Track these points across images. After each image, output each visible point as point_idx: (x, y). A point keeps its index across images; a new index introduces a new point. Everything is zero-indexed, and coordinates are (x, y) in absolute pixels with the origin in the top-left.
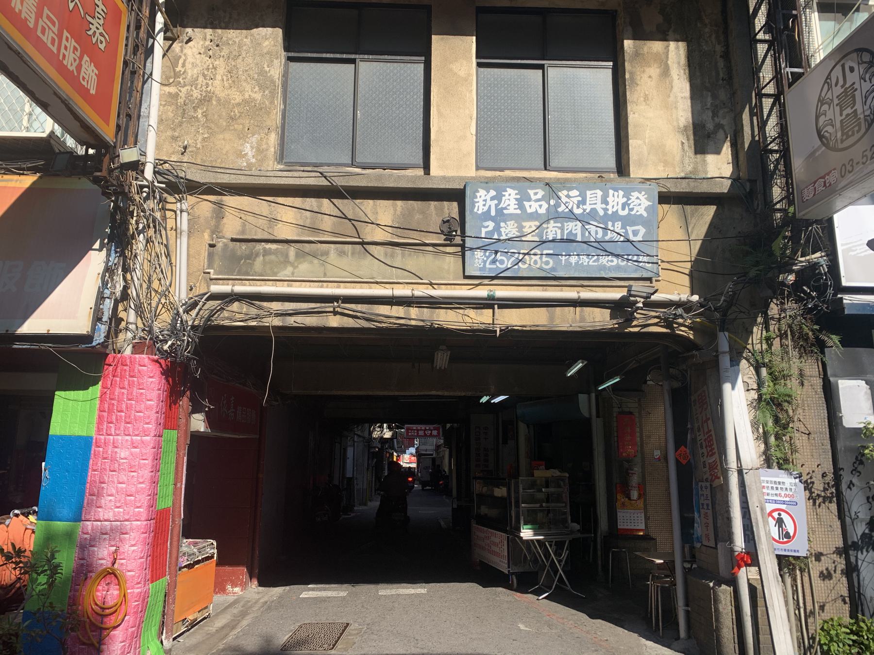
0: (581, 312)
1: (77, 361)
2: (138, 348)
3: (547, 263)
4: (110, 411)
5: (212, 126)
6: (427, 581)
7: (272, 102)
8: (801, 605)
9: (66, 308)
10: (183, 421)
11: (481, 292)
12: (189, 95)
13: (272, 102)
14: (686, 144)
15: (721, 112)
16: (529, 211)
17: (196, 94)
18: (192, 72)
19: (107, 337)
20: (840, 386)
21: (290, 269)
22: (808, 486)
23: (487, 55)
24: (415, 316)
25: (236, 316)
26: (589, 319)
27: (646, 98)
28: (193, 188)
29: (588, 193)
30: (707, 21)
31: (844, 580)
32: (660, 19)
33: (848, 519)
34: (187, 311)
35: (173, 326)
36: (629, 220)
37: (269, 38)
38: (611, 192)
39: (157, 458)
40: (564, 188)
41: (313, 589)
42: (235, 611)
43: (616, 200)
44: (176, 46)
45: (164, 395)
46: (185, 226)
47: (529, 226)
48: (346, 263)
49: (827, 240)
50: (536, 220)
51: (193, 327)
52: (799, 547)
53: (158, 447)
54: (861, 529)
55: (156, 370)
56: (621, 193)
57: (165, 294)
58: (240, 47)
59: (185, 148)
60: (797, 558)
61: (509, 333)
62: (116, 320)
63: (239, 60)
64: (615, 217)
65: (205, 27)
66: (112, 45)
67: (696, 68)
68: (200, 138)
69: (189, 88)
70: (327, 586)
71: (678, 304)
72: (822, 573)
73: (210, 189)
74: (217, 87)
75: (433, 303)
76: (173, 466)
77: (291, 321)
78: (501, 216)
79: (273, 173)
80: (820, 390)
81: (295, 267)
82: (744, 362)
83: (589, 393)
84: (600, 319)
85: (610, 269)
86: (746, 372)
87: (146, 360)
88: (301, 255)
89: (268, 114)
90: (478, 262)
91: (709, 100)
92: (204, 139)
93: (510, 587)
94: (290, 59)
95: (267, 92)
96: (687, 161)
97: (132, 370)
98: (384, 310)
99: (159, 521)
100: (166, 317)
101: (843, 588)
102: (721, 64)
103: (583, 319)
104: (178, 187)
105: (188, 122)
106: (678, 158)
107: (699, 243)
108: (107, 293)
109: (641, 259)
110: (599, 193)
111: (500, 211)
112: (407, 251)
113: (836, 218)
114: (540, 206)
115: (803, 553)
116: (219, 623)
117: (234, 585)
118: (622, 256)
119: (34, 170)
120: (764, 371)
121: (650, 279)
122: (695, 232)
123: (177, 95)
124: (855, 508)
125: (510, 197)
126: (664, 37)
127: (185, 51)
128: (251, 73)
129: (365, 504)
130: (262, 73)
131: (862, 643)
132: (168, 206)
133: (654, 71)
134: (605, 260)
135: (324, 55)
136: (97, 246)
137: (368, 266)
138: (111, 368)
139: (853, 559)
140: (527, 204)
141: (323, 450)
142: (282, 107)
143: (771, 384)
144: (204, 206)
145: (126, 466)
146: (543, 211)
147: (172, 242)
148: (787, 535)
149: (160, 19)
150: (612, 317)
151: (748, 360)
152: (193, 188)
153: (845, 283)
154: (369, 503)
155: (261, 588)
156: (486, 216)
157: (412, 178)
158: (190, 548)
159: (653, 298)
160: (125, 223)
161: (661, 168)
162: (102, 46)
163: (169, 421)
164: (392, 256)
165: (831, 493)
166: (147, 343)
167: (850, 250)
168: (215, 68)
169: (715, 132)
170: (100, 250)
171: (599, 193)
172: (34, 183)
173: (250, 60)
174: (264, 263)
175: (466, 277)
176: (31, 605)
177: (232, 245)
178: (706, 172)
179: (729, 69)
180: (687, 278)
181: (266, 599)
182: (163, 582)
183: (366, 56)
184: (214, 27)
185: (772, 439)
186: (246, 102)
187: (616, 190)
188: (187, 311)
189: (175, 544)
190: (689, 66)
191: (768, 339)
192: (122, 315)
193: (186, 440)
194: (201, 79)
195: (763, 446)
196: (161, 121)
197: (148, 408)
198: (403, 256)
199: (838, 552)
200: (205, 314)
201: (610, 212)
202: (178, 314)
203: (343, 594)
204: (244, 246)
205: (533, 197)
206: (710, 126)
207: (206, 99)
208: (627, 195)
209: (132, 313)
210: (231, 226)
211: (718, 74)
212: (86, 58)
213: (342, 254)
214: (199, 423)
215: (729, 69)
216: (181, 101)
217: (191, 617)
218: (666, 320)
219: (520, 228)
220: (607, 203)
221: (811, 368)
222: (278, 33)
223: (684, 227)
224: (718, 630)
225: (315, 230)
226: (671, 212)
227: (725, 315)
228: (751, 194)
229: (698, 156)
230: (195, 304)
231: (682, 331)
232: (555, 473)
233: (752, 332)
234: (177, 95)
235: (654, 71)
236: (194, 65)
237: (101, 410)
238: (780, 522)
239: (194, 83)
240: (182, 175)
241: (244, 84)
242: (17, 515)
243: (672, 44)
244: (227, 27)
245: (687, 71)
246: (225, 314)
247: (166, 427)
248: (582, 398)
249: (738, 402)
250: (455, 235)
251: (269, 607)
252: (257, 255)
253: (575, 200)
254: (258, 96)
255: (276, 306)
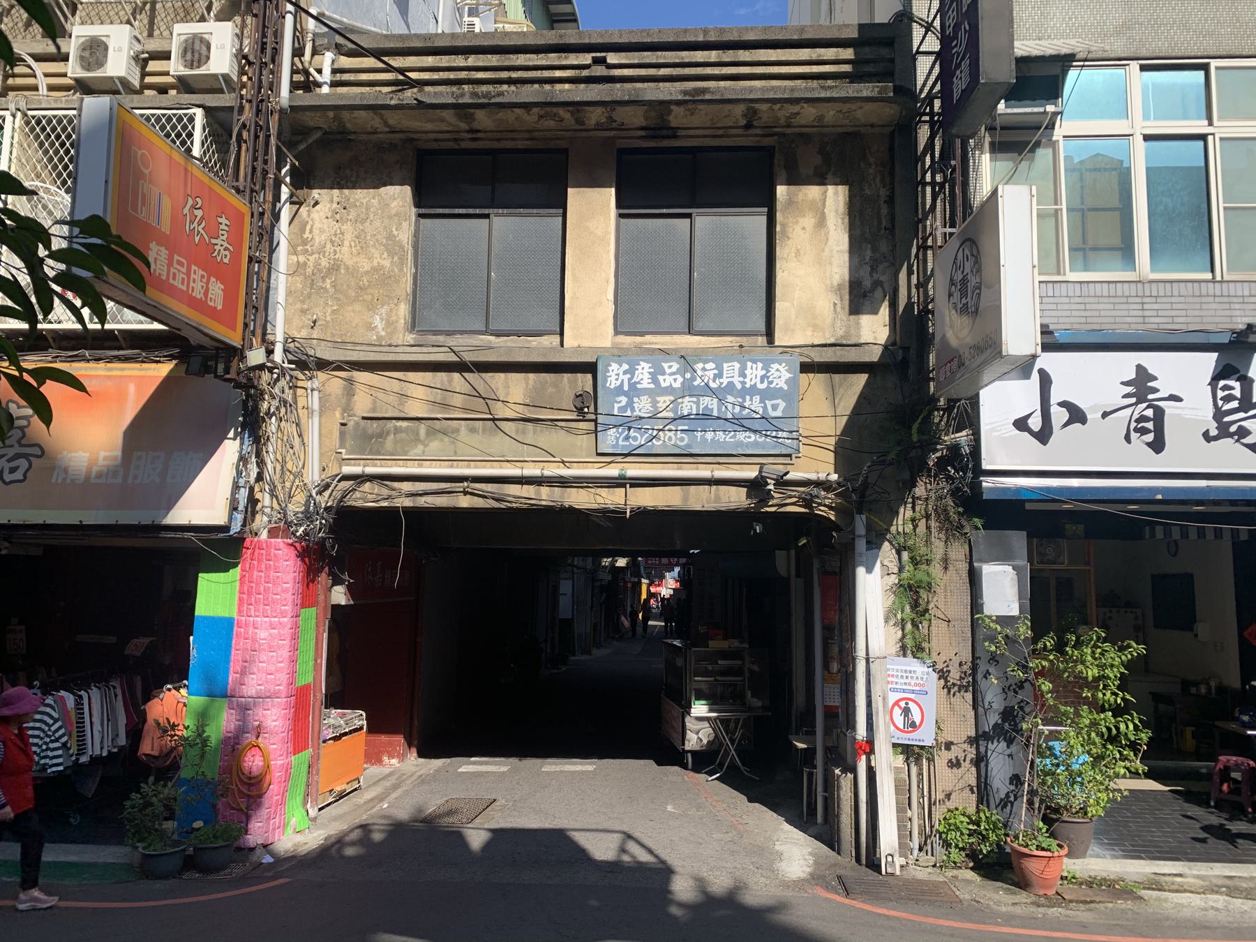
0: (717, 490)
1: (220, 547)
2: (273, 533)
3: (682, 439)
4: (250, 594)
5: (342, 297)
6: (601, 757)
7: (401, 270)
8: (926, 793)
9: (205, 501)
10: (321, 598)
11: (613, 471)
12: (317, 264)
13: (401, 270)
14: (839, 305)
15: (880, 268)
16: (663, 385)
17: (324, 263)
18: (319, 239)
19: (244, 525)
20: (984, 572)
21: (421, 447)
22: (943, 675)
23: (632, 202)
24: (545, 496)
25: (367, 497)
26: (724, 499)
27: (798, 252)
28: (322, 365)
29: (725, 365)
30: (872, 160)
31: (974, 769)
32: (818, 160)
33: (980, 710)
34: (320, 493)
35: (307, 511)
36: (768, 394)
37: (398, 197)
38: (749, 364)
39: (295, 637)
40: (700, 361)
41: (474, 763)
42: (388, 784)
43: (755, 372)
44: (303, 210)
45: (299, 576)
46: (316, 406)
47: (664, 401)
48: (475, 440)
49: (969, 418)
50: (671, 394)
51: (327, 509)
52: (925, 736)
53: (296, 626)
54: (994, 719)
55: (292, 553)
56: (760, 365)
57: (298, 475)
58: (368, 209)
59: (315, 322)
60: (922, 747)
61: (643, 514)
62: (252, 501)
63: (367, 224)
64: (753, 390)
65: (332, 188)
66: (236, 256)
67: (857, 216)
68: (329, 310)
69: (316, 256)
70: (491, 759)
71: (818, 484)
72: (950, 761)
73: (339, 366)
74: (346, 254)
75: (563, 482)
76: (313, 643)
77: (422, 502)
78: (634, 391)
79: (405, 345)
80: (965, 575)
81: (426, 446)
82: (886, 543)
83: (788, 550)
84: (736, 498)
85: (747, 445)
86: (887, 552)
87: (282, 545)
88: (432, 433)
89: (398, 282)
90: (611, 439)
91: (869, 253)
92: (334, 312)
93: (685, 767)
94: (420, 216)
95: (396, 258)
96: (838, 323)
97: (268, 554)
98: (514, 490)
99: (300, 697)
100: (300, 498)
101: (969, 775)
102: (885, 210)
103: (718, 499)
104: (305, 364)
105: (317, 294)
106: (829, 321)
107: (845, 419)
108: (242, 482)
109: (780, 434)
110: (737, 365)
111: (633, 386)
112: (539, 427)
113: (985, 395)
114: (675, 380)
115: (929, 741)
116: (368, 795)
117: (391, 756)
118: (760, 432)
119: (172, 357)
120: (905, 555)
121: (790, 456)
122: (842, 404)
123: (305, 264)
124: (988, 698)
125: (644, 372)
126: (822, 181)
127: (312, 215)
128: (379, 237)
129: (589, 653)
130: (391, 237)
131: (980, 833)
132: (300, 384)
133: (808, 221)
134: (742, 436)
135: (457, 211)
136: (231, 434)
137: (498, 443)
138: (249, 552)
139: (982, 749)
140: (661, 378)
141: (478, 618)
142: (413, 270)
143: (912, 568)
144: (333, 383)
145: (265, 647)
146: (677, 385)
147: (303, 421)
148: (913, 725)
149: (285, 192)
150: (749, 496)
151: (891, 543)
152: (322, 365)
153: (986, 466)
154: (595, 652)
155: (422, 760)
156: (619, 390)
157: (542, 347)
158: (337, 719)
159: (788, 477)
160: (256, 408)
161: (809, 333)
162: (226, 261)
163: (307, 600)
164: (524, 432)
165: (966, 682)
166: (282, 528)
167: (993, 430)
168: (342, 233)
169: (872, 290)
170: (234, 439)
171: (737, 365)
172: (171, 371)
173: (378, 223)
174: (395, 442)
175: (599, 454)
176: (186, 773)
177: (363, 422)
178: (859, 336)
179: (892, 217)
180: (832, 454)
181: (423, 772)
182: (306, 755)
183: (500, 211)
184: (341, 187)
185: (909, 627)
186: (375, 270)
187: (754, 362)
188: (320, 493)
189: (317, 718)
190: (849, 214)
191: (913, 520)
192: (258, 496)
193: (325, 615)
194: (329, 245)
195: (900, 633)
196: (289, 293)
197: (285, 591)
198: (535, 432)
199: (973, 741)
200: (338, 494)
201: (748, 386)
202: (311, 496)
203: (590, 768)
204: (375, 424)
205: (668, 371)
206: (867, 283)
207: (335, 268)
208: (766, 368)
209: (267, 496)
210: (362, 404)
211: (880, 222)
212: (213, 279)
213: (473, 430)
214: (339, 596)
215: (892, 217)
216: (309, 271)
217: (338, 789)
218: (804, 500)
219: (654, 403)
220: (745, 376)
221: (958, 552)
222: (407, 190)
223: (830, 398)
224: (838, 816)
225: (445, 406)
226: (818, 379)
227: (863, 496)
228: (903, 366)
229: (852, 317)
230: (327, 486)
231: (822, 511)
232: (736, 643)
233: (897, 513)
234: (305, 264)
235: (808, 221)
236: (322, 231)
237: (241, 592)
238: (906, 711)
239: (321, 251)
240: (311, 352)
241: (373, 250)
242: (169, 690)
243: (831, 188)
244: (354, 187)
245: (847, 221)
246: (358, 494)
247: (303, 606)
248: (780, 555)
249: (873, 589)
250: (586, 408)
251: (422, 780)
252: (388, 433)
253: (711, 374)
254: (387, 263)
255: (406, 486)
